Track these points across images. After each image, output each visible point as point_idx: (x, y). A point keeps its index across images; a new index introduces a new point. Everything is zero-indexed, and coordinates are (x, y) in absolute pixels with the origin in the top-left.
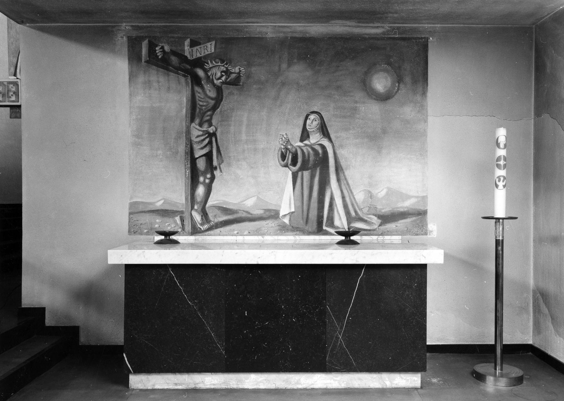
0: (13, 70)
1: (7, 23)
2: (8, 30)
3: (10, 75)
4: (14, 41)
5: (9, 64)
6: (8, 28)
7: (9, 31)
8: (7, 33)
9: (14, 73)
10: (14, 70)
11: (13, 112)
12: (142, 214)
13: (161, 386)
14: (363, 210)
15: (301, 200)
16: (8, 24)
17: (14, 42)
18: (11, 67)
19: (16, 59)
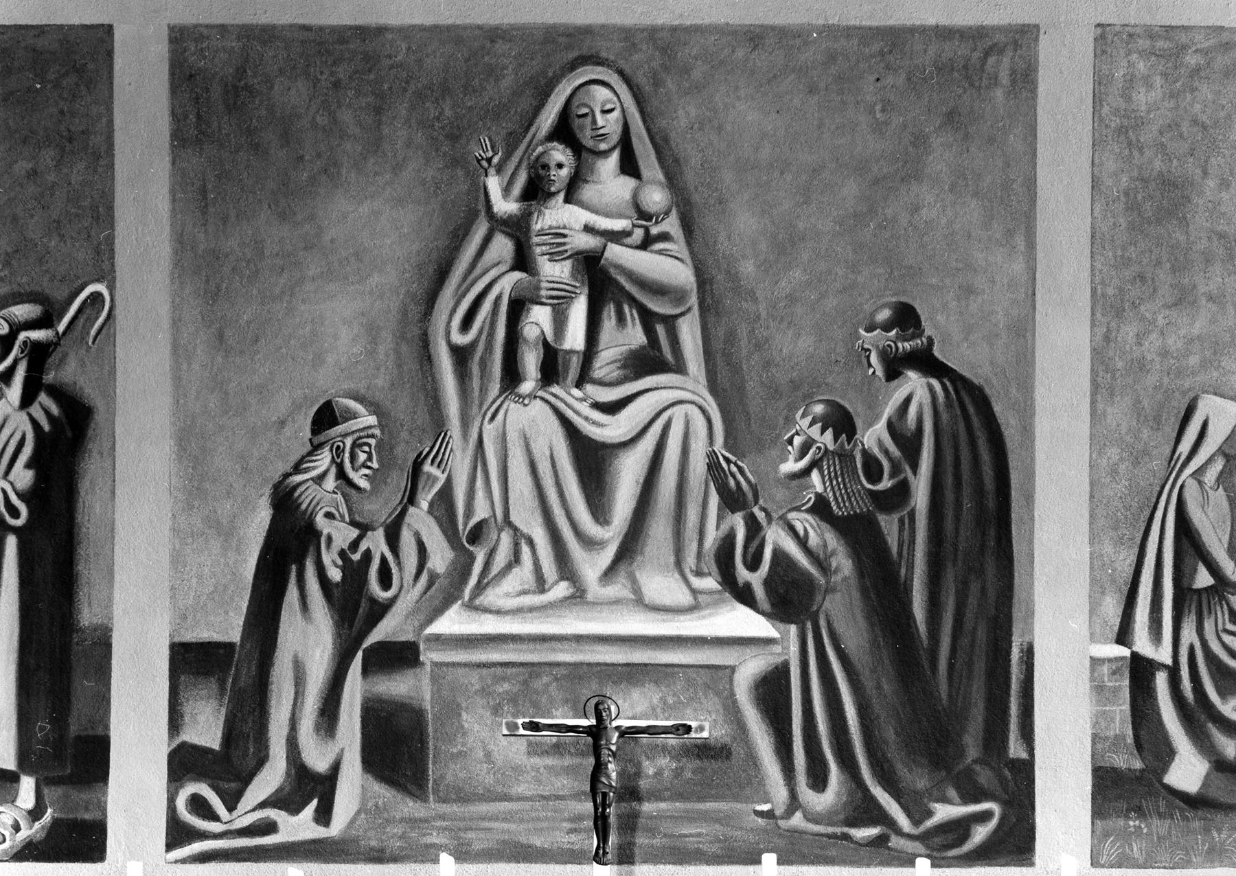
0: (1112, 609)
1: (1093, 365)
2: (1093, 403)
3: (1093, 638)
4: (1121, 459)
5: (1093, 581)
6: (1094, 394)
7: (1100, 406)
8: (1087, 417)
9: (1116, 629)
10: (1120, 612)
11: (1107, 835)
12: (633, 434)
13: (839, 489)
14: (584, 155)
15: (560, 472)
16: (1092, 370)
17: (1122, 467)
18: (1103, 593)
19: (1133, 558)
